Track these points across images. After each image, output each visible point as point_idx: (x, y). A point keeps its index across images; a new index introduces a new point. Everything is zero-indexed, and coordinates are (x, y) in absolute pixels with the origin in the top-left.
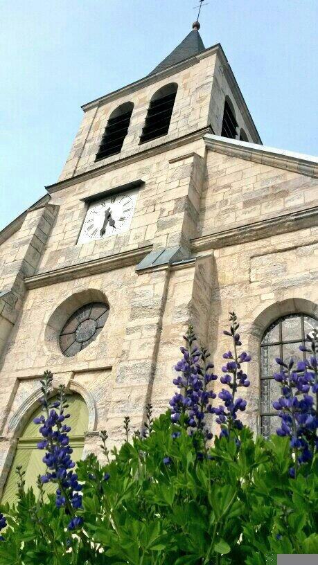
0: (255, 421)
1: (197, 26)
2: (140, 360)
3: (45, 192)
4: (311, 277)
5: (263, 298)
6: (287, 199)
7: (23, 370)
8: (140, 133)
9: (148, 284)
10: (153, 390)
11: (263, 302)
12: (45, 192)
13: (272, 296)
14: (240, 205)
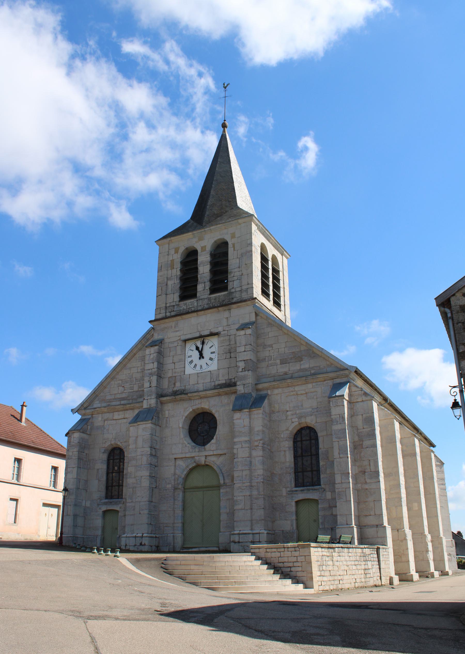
0: (292, 476)
1: (225, 120)
2: (244, 458)
3: (150, 326)
4: (313, 411)
5: (293, 420)
6: (302, 362)
7: (176, 454)
8: (208, 285)
9: (240, 419)
10: (291, 443)
11: (293, 422)
12: (150, 326)
13: (297, 420)
14: (278, 361)
